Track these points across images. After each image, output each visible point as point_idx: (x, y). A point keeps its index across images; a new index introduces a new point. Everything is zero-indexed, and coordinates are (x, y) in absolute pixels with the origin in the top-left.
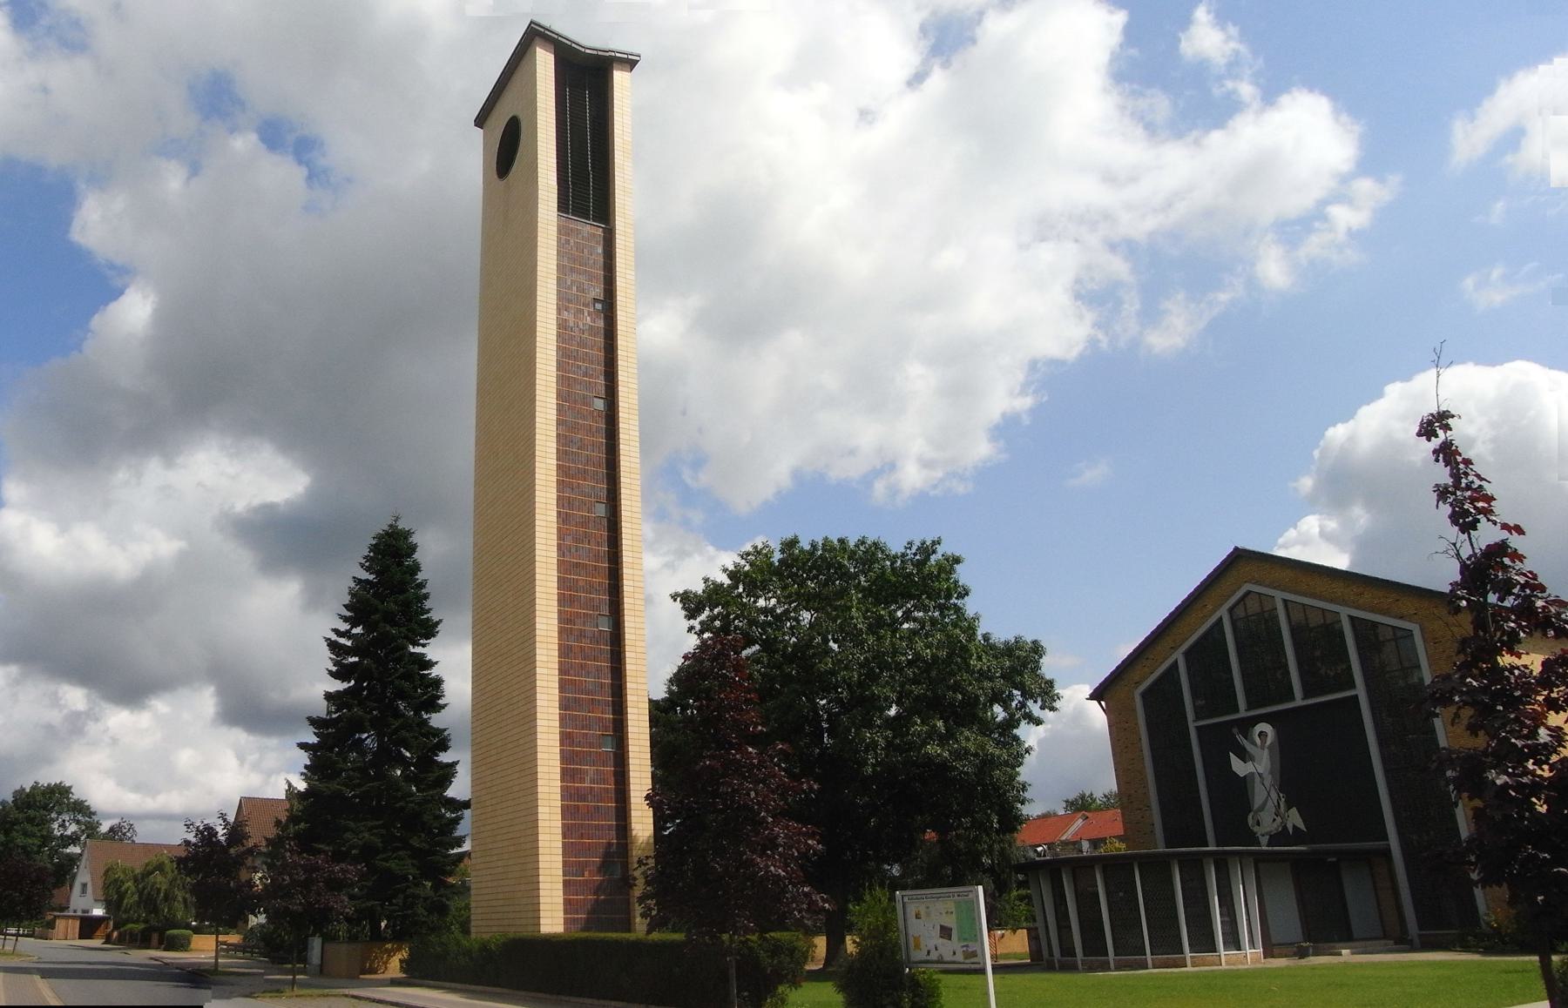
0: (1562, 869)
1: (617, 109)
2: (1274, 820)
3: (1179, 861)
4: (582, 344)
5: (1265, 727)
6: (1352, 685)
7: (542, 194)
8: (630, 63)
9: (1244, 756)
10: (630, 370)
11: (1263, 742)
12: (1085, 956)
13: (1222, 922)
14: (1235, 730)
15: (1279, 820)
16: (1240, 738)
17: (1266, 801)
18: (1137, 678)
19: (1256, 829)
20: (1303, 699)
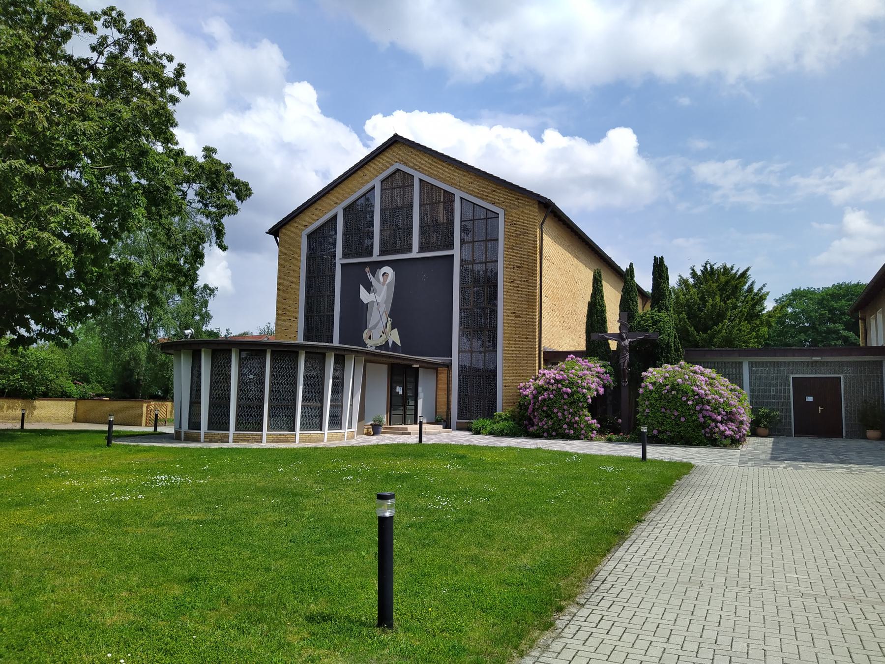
2: (381, 336)
3: (306, 353)
9: (369, 288)
11: (385, 281)
12: (208, 430)
13: (331, 406)
14: (367, 270)
15: (384, 336)
16: (370, 276)
18: (306, 222)
20: (420, 252)
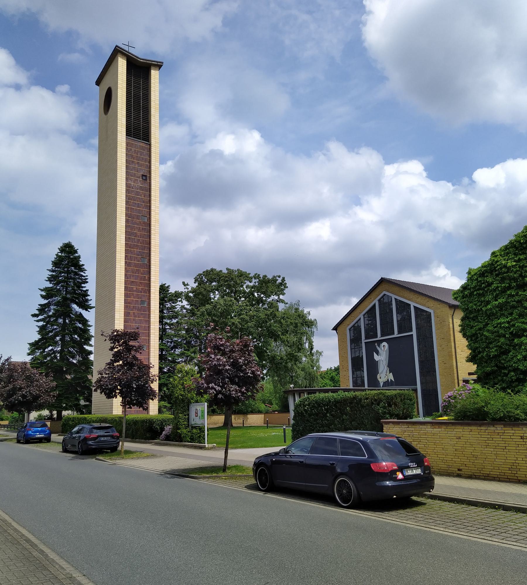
0: (346, 505)
1: (152, 89)
4: (137, 193)
5: (385, 343)
6: (411, 330)
7: (119, 128)
8: (159, 66)
9: (378, 353)
10: (156, 205)
11: (384, 349)
14: (376, 344)
16: (377, 347)
17: (383, 371)
19: (379, 380)
